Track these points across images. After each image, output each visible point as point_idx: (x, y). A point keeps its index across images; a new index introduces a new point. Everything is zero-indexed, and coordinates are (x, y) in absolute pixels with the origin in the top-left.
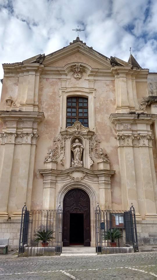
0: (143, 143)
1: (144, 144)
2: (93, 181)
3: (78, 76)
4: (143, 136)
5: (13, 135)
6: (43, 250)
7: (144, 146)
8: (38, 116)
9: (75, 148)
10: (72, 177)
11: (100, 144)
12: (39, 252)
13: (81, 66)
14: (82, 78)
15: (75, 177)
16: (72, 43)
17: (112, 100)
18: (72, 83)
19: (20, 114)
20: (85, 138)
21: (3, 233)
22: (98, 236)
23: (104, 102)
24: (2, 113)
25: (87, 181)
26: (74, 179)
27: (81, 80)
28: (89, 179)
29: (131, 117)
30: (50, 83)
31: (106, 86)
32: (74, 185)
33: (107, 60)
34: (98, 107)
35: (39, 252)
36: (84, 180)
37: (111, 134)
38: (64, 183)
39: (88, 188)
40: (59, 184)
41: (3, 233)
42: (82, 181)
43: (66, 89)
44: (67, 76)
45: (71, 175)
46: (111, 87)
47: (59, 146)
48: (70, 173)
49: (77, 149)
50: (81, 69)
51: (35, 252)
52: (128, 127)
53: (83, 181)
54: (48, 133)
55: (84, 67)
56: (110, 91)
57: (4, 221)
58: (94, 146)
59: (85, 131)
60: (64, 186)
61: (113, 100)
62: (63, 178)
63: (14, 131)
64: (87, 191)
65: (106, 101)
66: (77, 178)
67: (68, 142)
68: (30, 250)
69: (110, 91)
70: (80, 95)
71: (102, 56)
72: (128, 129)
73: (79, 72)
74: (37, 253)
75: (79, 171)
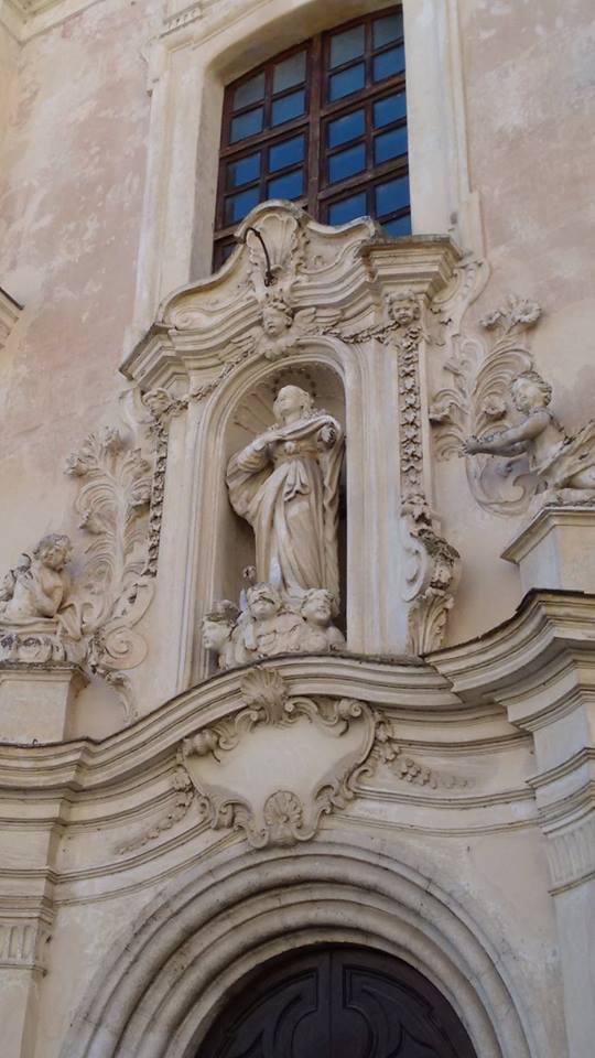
2: (466, 805)
10: (219, 802)
11: (539, 336)
15: (254, 795)
20: (355, 340)
25: (394, 813)
36: (359, 808)
38: (138, 886)
40: (91, 910)
43: (198, 13)
45: (204, 773)
48: (187, 749)
58: (469, 386)
60: (146, 925)
62: (133, 829)
64: (389, 930)
66: (283, 805)
75: (268, 715)
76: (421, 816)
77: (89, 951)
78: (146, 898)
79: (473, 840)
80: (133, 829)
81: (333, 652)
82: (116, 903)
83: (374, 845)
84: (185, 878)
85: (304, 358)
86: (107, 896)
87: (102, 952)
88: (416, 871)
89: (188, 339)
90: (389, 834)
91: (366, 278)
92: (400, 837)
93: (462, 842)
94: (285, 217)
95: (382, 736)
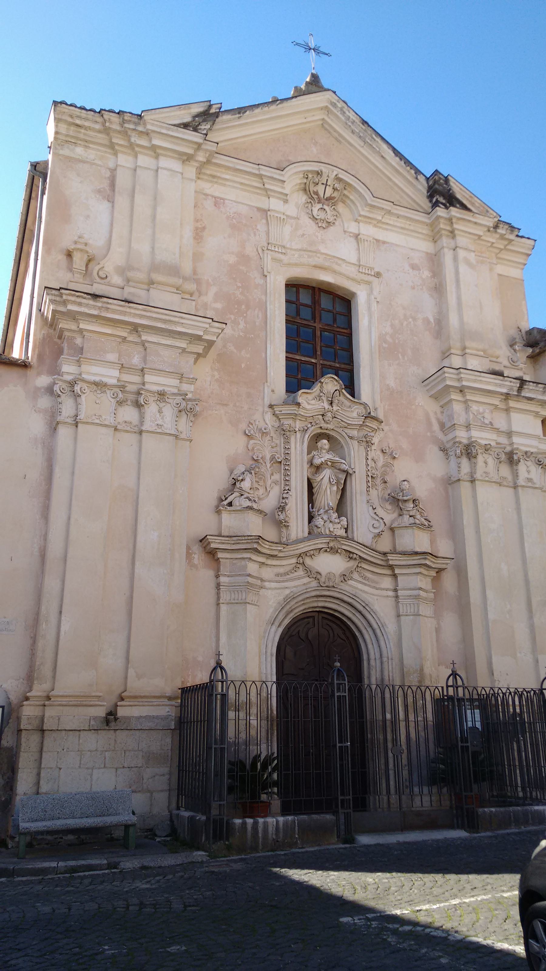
0: (526, 475)
1: (530, 480)
3: (322, 215)
4: (529, 454)
5: (109, 393)
6: (297, 828)
7: (530, 484)
8: (206, 331)
9: (318, 468)
10: (313, 572)
12: (281, 835)
13: (338, 179)
14: (337, 223)
16: (301, 89)
17: (429, 322)
18: (303, 235)
19: (141, 316)
21: (88, 768)
22: (517, 764)
23: (405, 323)
24: (73, 299)
25: (360, 586)
26: (319, 576)
27: (332, 228)
28: (364, 581)
29: (500, 386)
30: (228, 218)
31: (411, 270)
32: (315, 599)
33: (417, 178)
34: (388, 338)
35: (281, 835)
36: (351, 582)
37: (429, 434)
39: (360, 612)
40: (270, 591)
41: (88, 768)
42: (343, 586)
44: (287, 206)
46: (424, 277)
47: (268, 457)
49: (327, 473)
50: (335, 189)
51: (270, 836)
52: (484, 417)
53: (347, 588)
54: (226, 405)
55: (347, 185)
56: (422, 289)
57: (92, 723)
59: (353, 414)
61: (432, 320)
63: (111, 377)
65: (410, 320)
67: (298, 448)
68: (249, 827)
69: (422, 289)
70: (329, 284)
71: (403, 162)
72: (484, 423)
73: (327, 199)
74: (274, 837)
75: (333, 551)
76: (366, 588)
77: (270, 603)
78: (287, 592)
79: (378, 598)
80: (281, 570)
81: (347, 538)
82: (278, 591)
83: (353, 593)
84: (300, 589)
85: (331, 433)
86: (276, 589)
87: (275, 605)
88: (364, 602)
89: (303, 411)
90: (357, 591)
91: (361, 423)
92: (360, 593)
93: (376, 597)
94: (336, 383)
95: (359, 565)
